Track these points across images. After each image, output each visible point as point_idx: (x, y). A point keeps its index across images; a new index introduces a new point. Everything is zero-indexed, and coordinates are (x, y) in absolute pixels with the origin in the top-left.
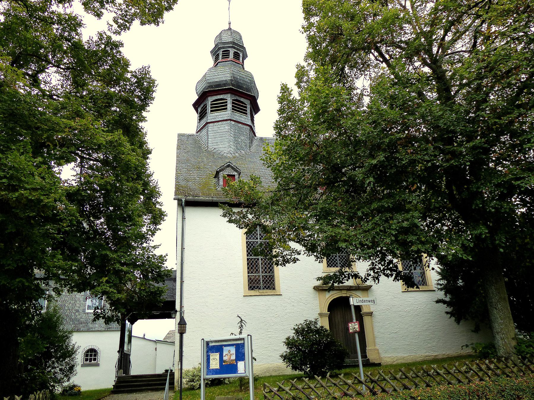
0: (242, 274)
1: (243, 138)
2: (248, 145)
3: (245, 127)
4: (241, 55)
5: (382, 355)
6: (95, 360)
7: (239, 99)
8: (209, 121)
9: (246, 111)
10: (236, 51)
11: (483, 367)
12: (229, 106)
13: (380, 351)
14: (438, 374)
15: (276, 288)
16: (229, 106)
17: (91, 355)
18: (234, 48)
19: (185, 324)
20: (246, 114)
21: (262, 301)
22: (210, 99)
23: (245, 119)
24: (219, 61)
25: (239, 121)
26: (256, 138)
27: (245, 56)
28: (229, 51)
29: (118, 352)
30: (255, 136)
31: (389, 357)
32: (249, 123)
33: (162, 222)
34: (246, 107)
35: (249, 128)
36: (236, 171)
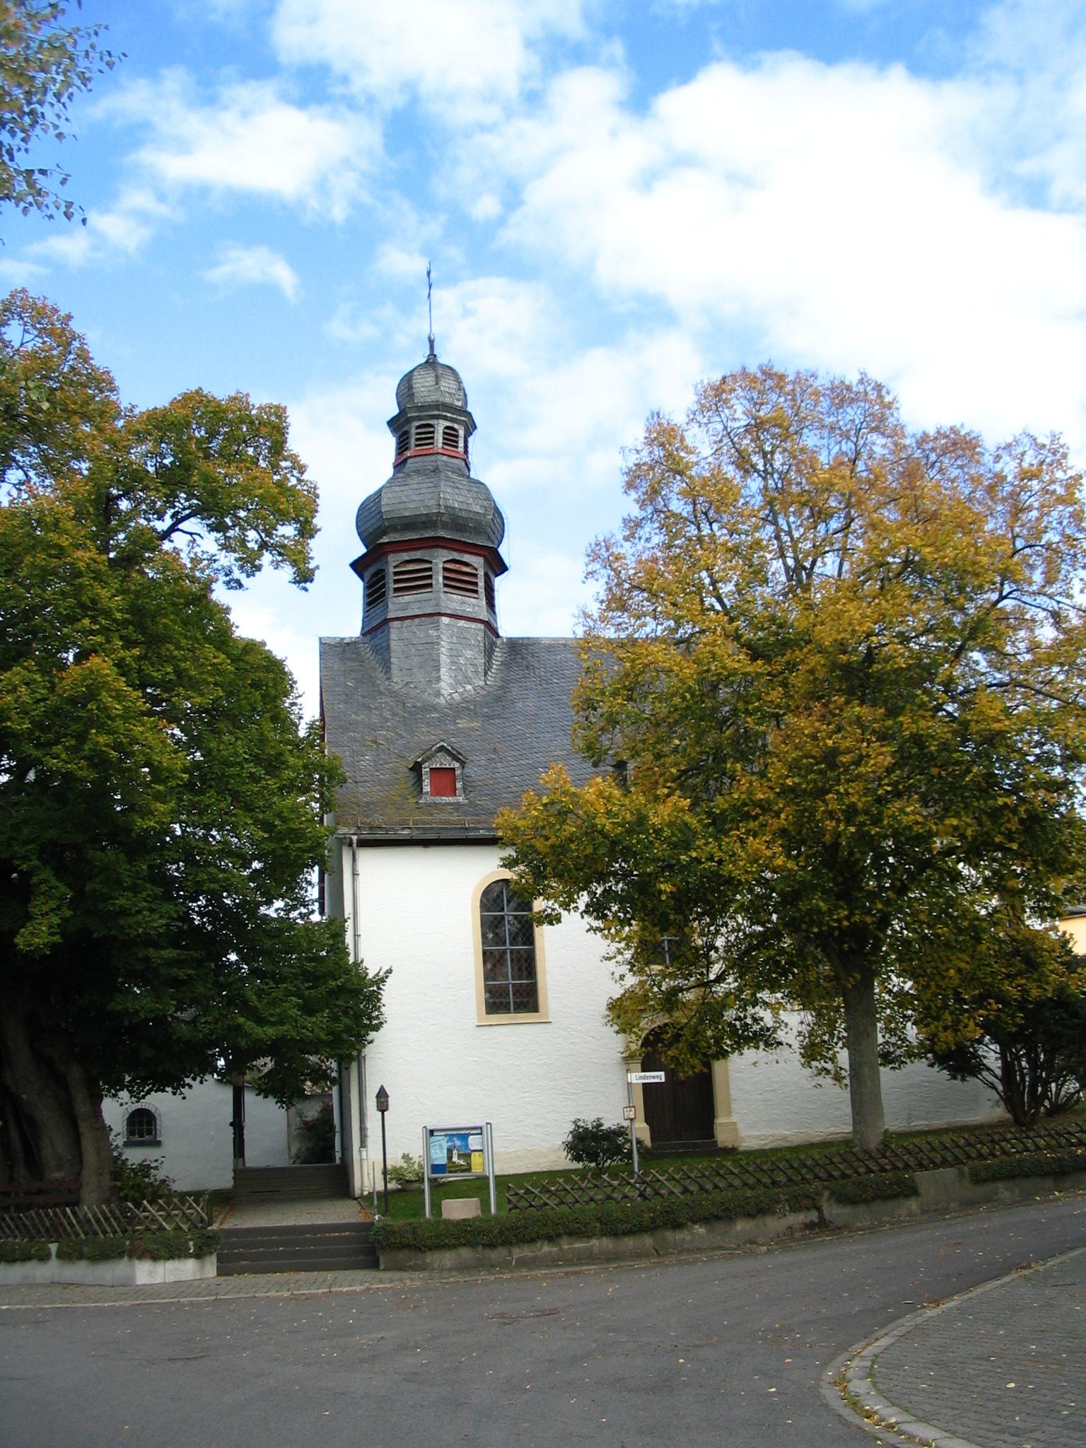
0: (473, 983)
1: (468, 653)
2: (481, 669)
3: (473, 625)
4: (461, 433)
5: (743, 1134)
6: (149, 1133)
7: (456, 556)
8: (390, 615)
9: (476, 584)
10: (448, 424)
11: (1030, 1144)
12: (439, 579)
13: (739, 1126)
14: (672, 1193)
15: (541, 1008)
16: (439, 579)
17: (141, 1124)
18: (445, 418)
19: (387, 1096)
20: (476, 592)
21: (514, 1032)
22: (393, 560)
23: (476, 605)
24: (408, 454)
25: (460, 613)
26: (499, 642)
27: (470, 427)
28: (432, 426)
29: (231, 1124)
30: (498, 636)
31: (757, 1137)
32: (484, 615)
33: (364, 965)
34: (475, 576)
35: (482, 626)
36: (458, 760)
